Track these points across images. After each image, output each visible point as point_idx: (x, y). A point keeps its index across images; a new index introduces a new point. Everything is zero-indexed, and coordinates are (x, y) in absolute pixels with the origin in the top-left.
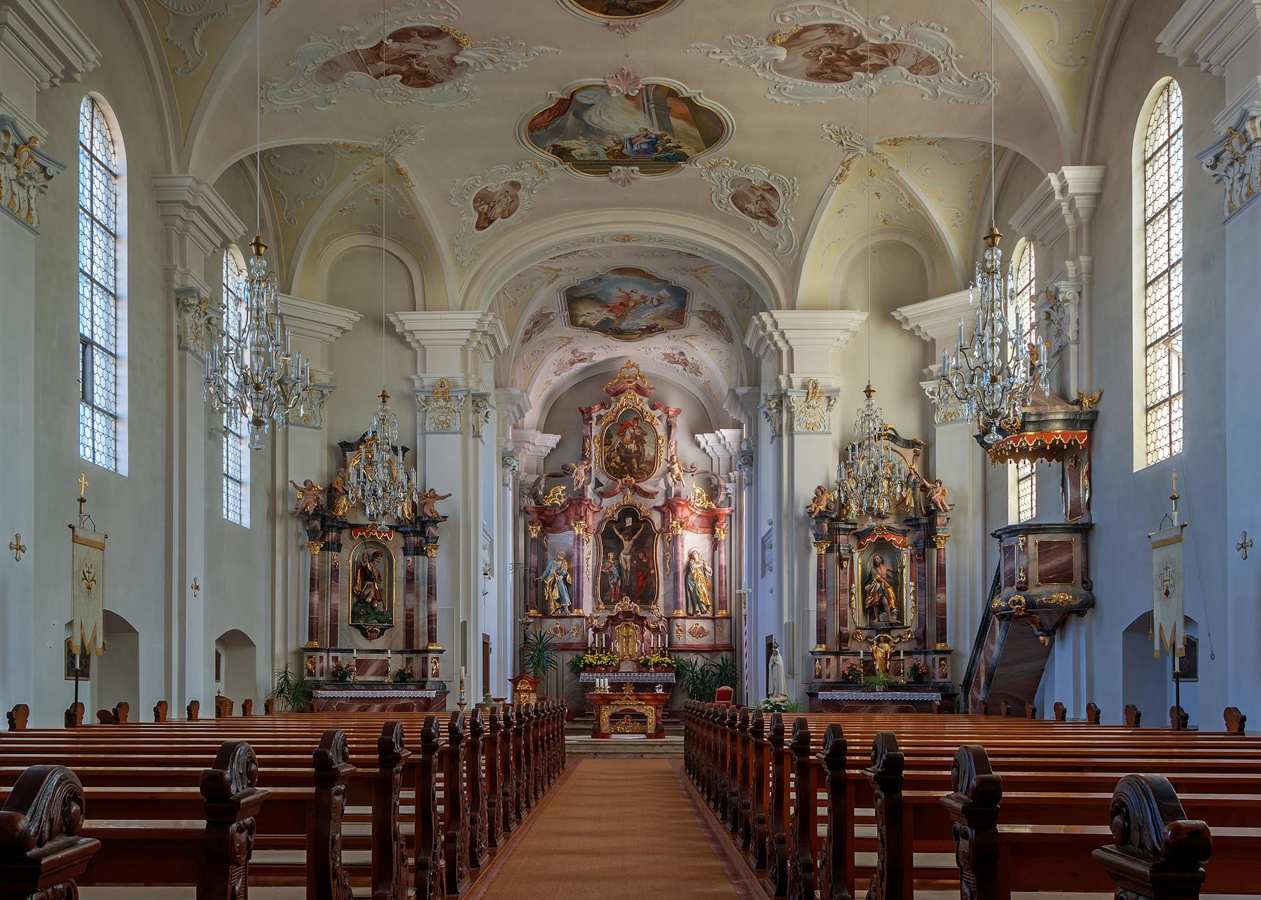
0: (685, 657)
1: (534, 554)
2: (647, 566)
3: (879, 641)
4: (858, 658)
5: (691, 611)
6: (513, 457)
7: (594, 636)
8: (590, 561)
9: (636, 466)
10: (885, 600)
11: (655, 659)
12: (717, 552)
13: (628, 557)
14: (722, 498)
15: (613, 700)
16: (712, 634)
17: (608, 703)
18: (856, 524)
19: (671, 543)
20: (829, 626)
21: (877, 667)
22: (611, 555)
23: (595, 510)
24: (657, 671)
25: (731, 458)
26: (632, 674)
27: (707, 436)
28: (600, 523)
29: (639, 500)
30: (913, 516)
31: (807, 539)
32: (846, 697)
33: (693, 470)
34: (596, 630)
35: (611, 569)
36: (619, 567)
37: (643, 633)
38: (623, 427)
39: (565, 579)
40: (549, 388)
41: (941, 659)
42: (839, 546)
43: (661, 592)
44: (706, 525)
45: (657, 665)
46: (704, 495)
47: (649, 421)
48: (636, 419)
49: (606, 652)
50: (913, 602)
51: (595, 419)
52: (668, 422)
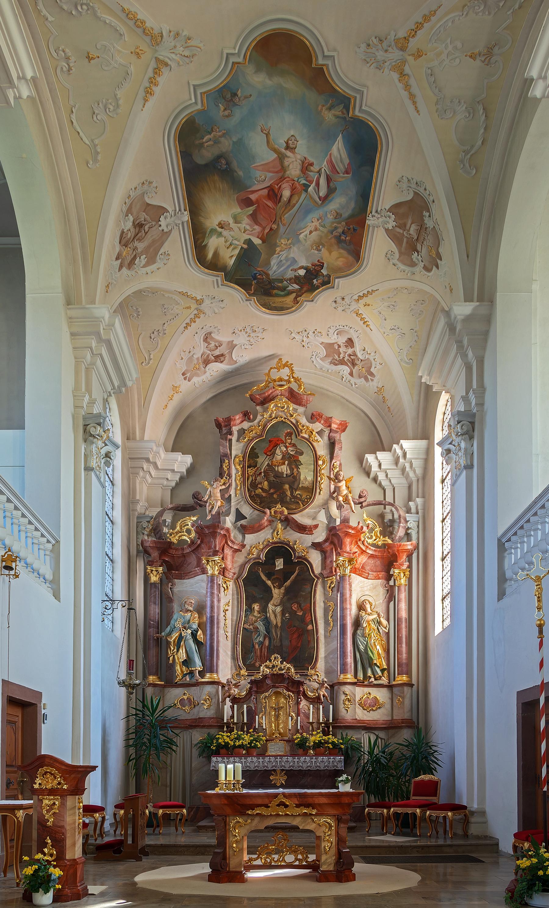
0: (354, 736)
1: (155, 603)
2: (302, 620)
5: (361, 676)
6: (99, 424)
7: (232, 708)
8: (229, 613)
9: (289, 493)
11: (316, 737)
12: (392, 604)
13: (279, 609)
14: (401, 532)
15: (252, 807)
16: (388, 706)
17: (242, 814)
19: (335, 589)
22: (256, 607)
23: (235, 547)
24: (317, 755)
25: (410, 487)
26: (285, 759)
27: (380, 455)
28: (242, 566)
29: (292, 536)
33: (362, 500)
34: (235, 700)
35: (256, 624)
36: (267, 622)
37: (298, 703)
38: (274, 444)
39: (194, 635)
40: (177, 398)
43: (322, 653)
44: (379, 568)
45: (318, 745)
46: (378, 529)
47: (306, 436)
48: (290, 434)
49: (248, 730)
51: (235, 434)
52: (329, 438)
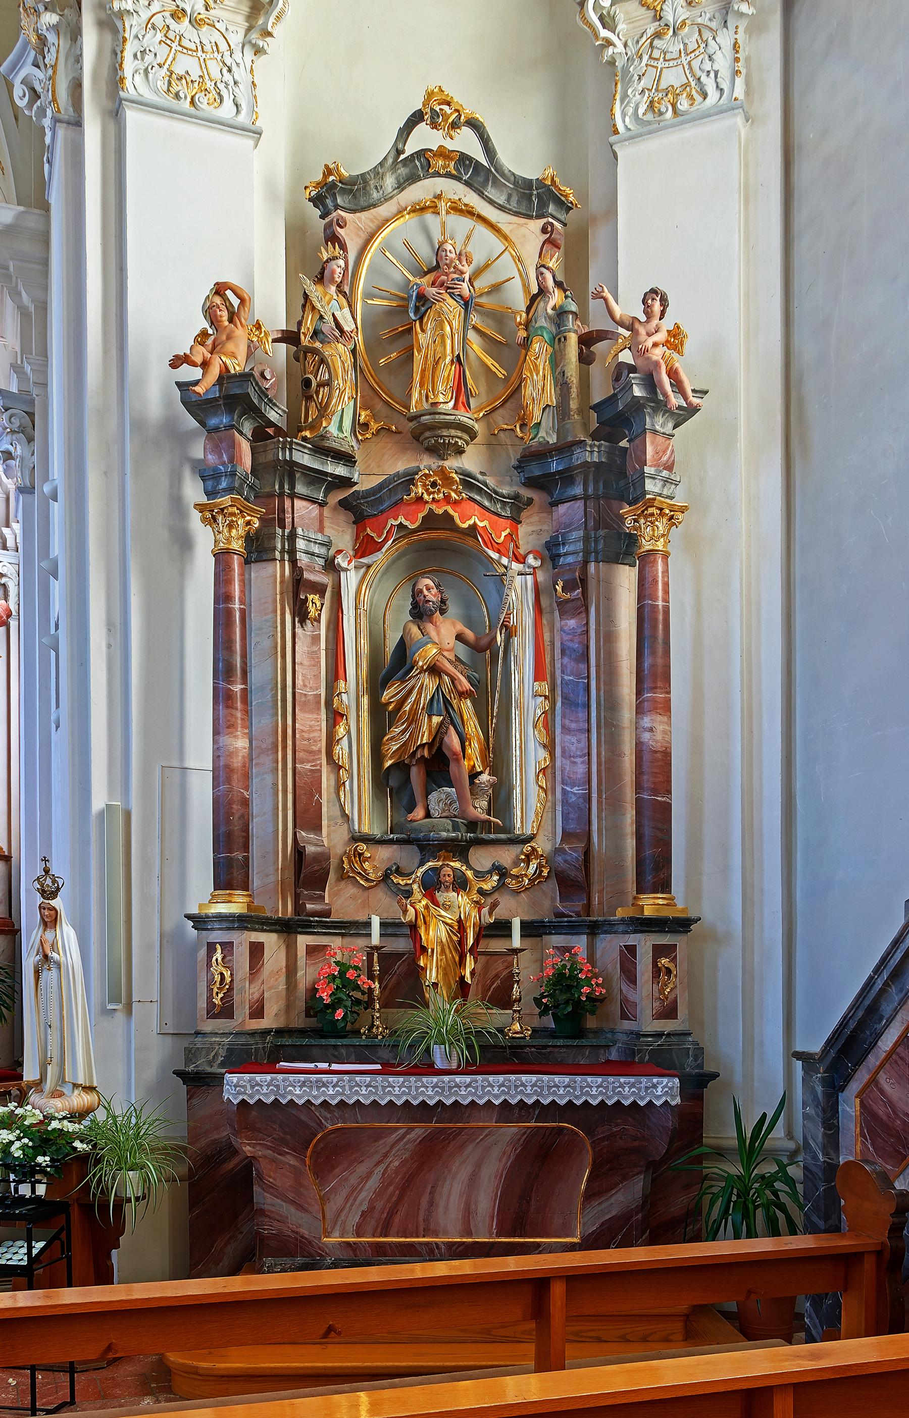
3: (431, 886)
4: (361, 942)
10: (454, 741)
18: (347, 459)
20: (259, 827)
21: (432, 975)
30: (553, 439)
31: (177, 503)
32: (332, 1095)
41: (659, 951)
42: (293, 536)
50: (543, 754)
